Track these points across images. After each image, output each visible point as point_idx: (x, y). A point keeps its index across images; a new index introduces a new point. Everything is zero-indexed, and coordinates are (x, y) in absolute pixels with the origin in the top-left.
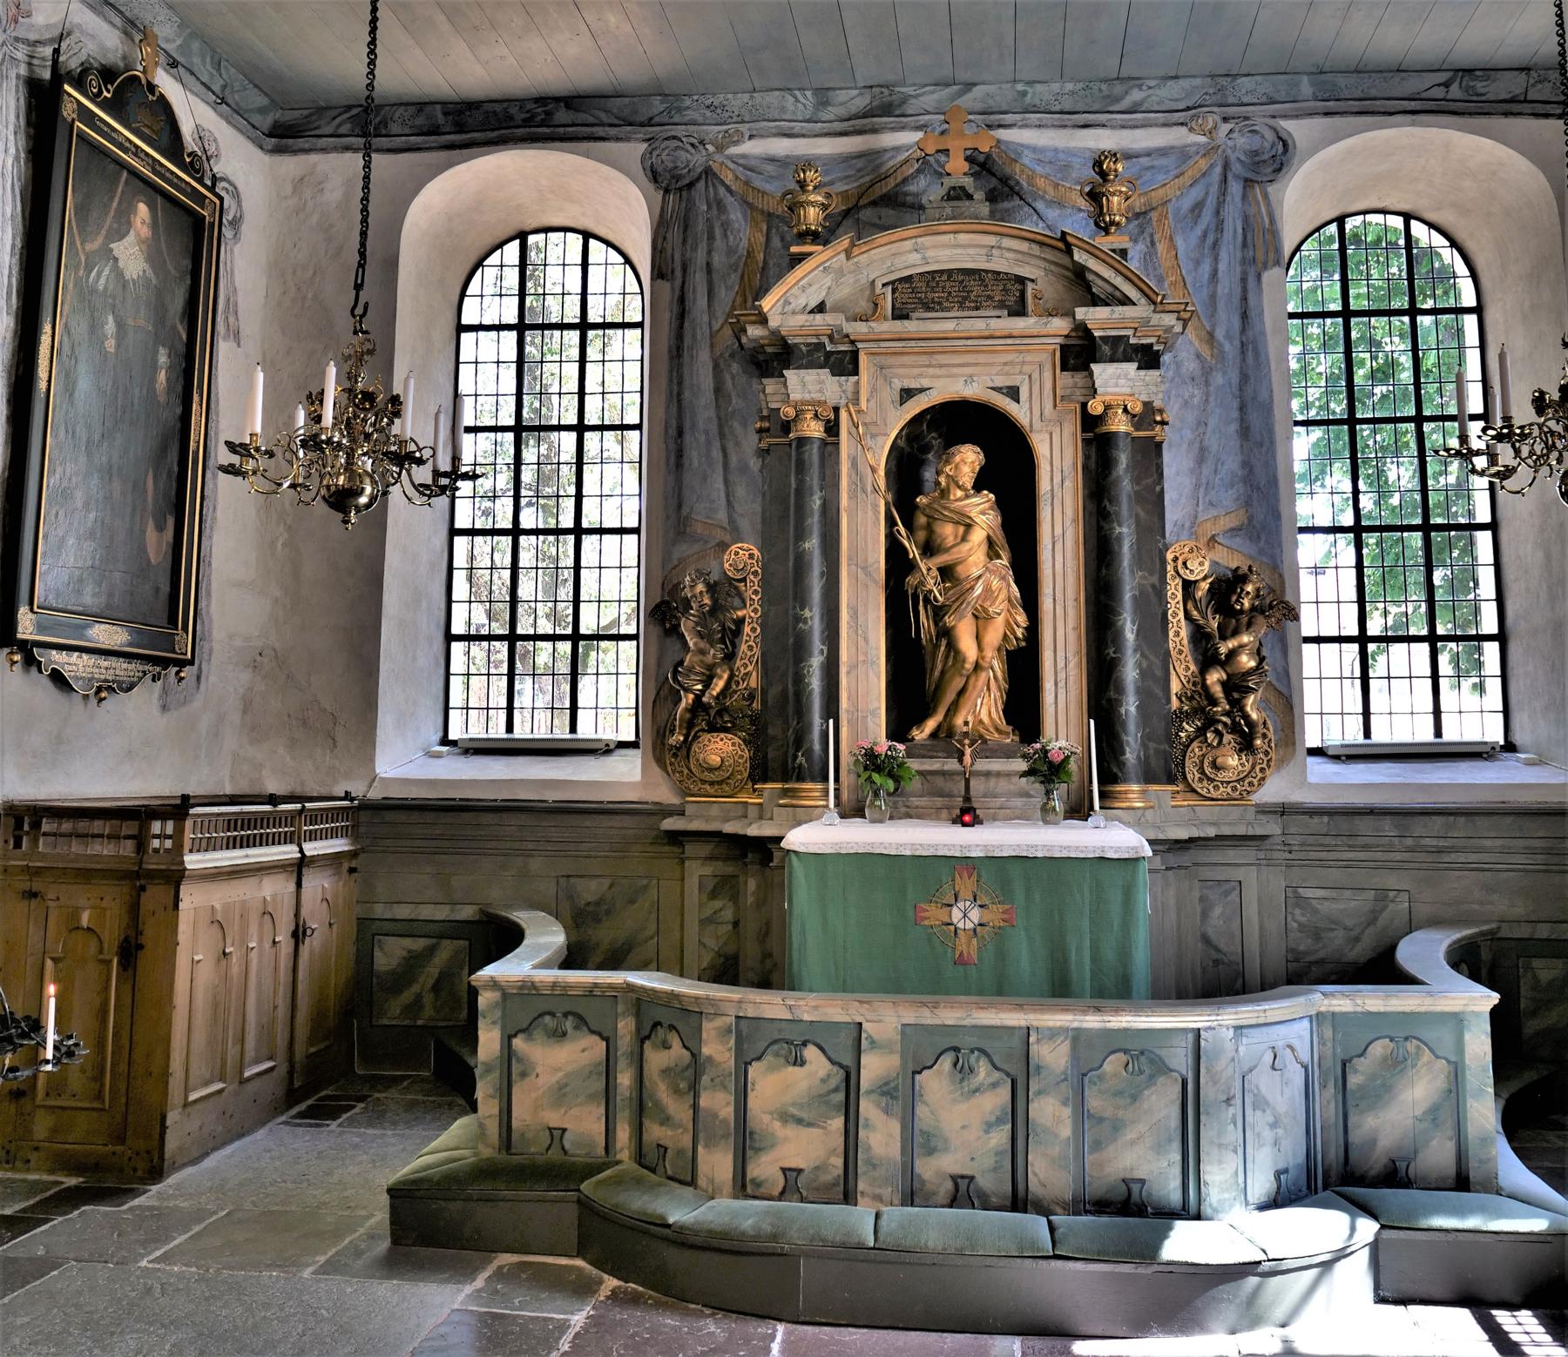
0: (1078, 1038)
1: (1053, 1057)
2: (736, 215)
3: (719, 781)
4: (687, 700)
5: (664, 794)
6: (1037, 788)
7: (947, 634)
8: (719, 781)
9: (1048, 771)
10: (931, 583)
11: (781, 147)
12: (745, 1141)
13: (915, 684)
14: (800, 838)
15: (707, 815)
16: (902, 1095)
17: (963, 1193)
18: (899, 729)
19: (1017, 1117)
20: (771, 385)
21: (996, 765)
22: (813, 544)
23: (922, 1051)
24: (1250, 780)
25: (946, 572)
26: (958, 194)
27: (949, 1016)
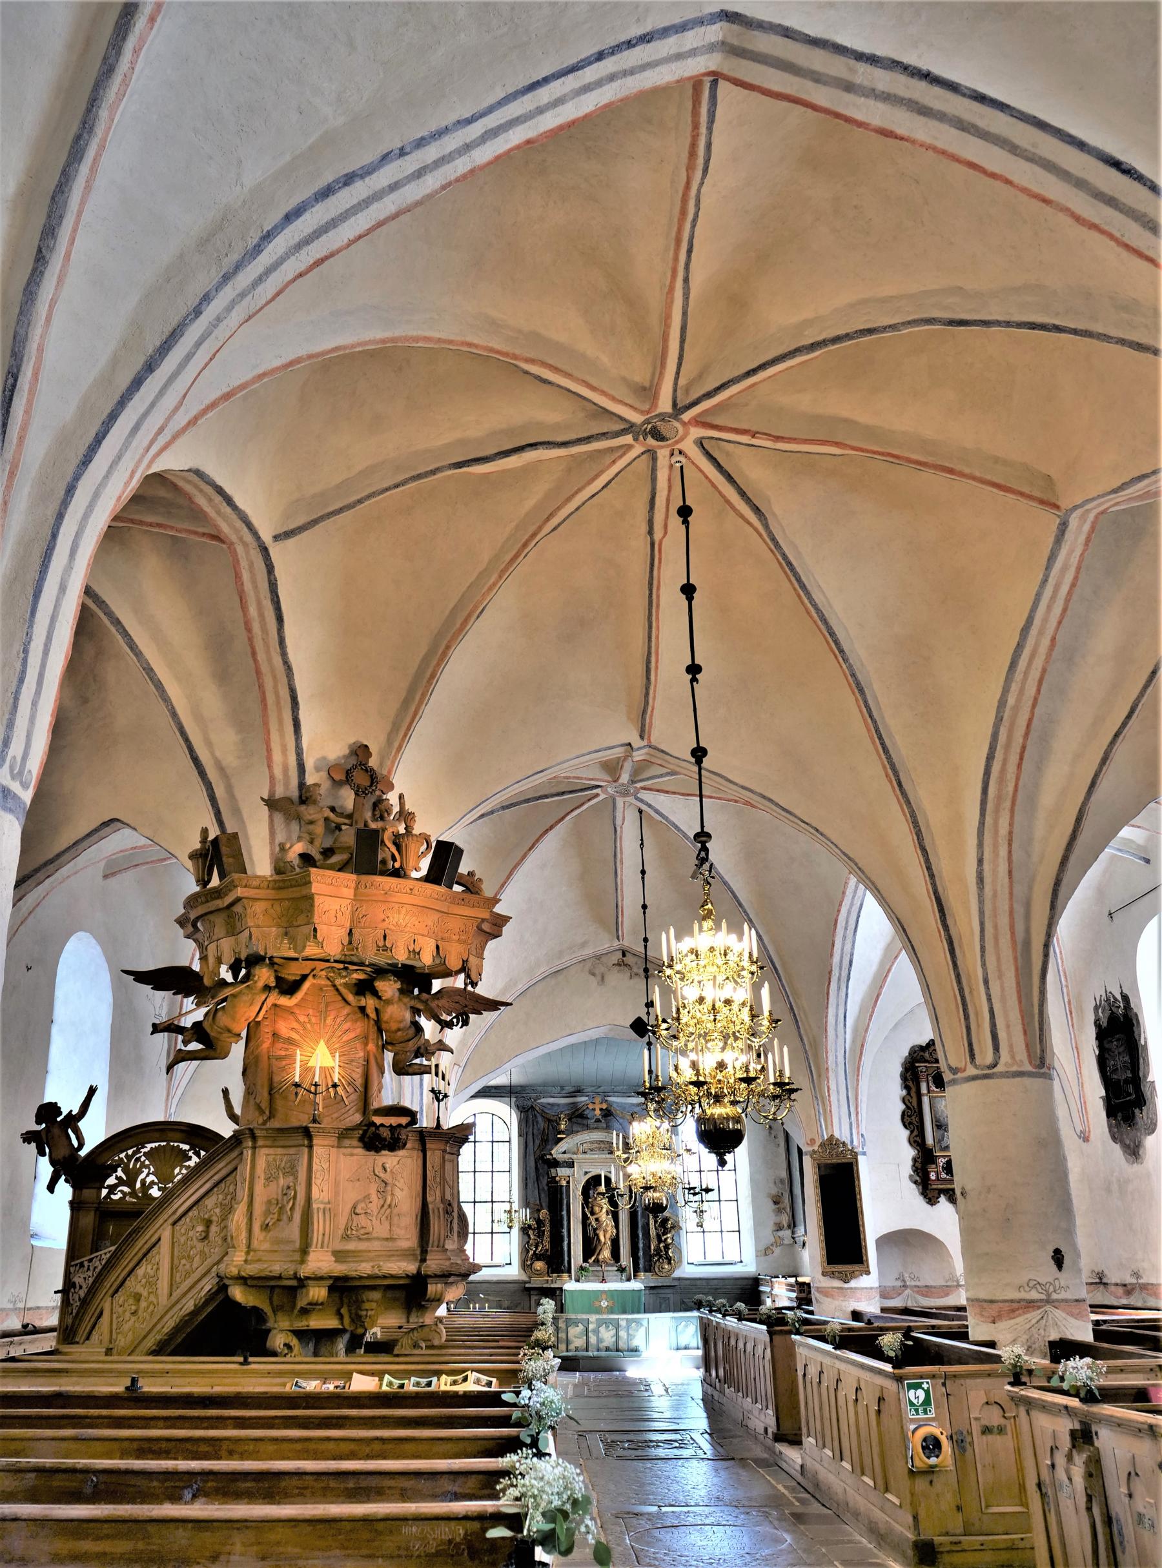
0: (627, 1320)
1: (623, 1323)
2: (540, 1119)
3: (539, 1274)
4: (531, 1252)
5: (524, 1278)
6: (619, 1273)
7: (597, 1235)
8: (539, 1274)
9: (622, 1270)
10: (594, 1223)
11: (551, 1100)
12: (568, 1342)
13: (590, 1248)
14: (566, 1287)
15: (537, 1282)
16: (596, 1332)
17: (608, 1349)
18: (585, 1260)
19: (617, 1335)
20: (553, 1170)
21: (609, 1268)
22: (564, 1213)
23: (600, 1322)
24: (671, 1271)
25: (597, 1220)
26: (598, 1121)
27: (605, 1316)
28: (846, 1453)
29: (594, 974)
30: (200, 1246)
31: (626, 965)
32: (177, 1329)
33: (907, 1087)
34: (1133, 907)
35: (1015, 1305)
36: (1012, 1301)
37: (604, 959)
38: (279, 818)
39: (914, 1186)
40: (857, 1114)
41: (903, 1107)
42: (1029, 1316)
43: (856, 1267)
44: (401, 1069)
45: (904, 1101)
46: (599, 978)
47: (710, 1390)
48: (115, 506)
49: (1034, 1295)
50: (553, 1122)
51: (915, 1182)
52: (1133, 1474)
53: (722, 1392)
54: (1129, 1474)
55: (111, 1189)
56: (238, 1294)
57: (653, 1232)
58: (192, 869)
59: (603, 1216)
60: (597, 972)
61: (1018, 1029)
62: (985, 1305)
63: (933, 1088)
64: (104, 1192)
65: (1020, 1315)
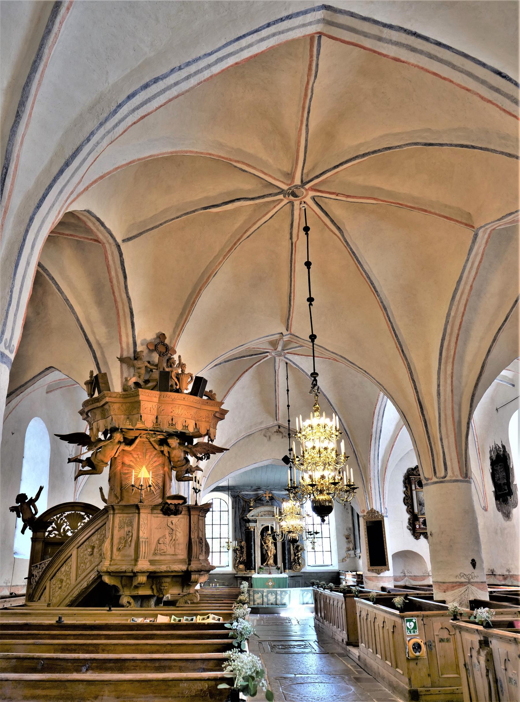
0: (281, 591)
1: (279, 592)
2: (241, 501)
3: (241, 570)
4: (238, 561)
5: (235, 572)
6: (277, 570)
7: (267, 553)
8: (241, 570)
9: (278, 569)
10: (266, 548)
11: (247, 493)
12: (254, 601)
13: (264, 559)
14: (253, 576)
15: (240, 574)
16: (267, 596)
17: (272, 604)
18: (262, 564)
19: (276, 598)
20: (247, 524)
21: (273, 568)
22: (253, 543)
23: (269, 592)
24: (300, 569)
25: (267, 546)
26: (268, 502)
27: (271, 589)
28: (379, 651)
29: (266, 436)
30: (89, 558)
31: (280, 432)
32: (79, 595)
33: (406, 487)
34: (507, 406)
35: (454, 584)
36: (453, 582)
37: (270, 429)
38: (125, 366)
39: (409, 531)
40: (384, 499)
41: (404, 496)
42: (460, 589)
43: (383, 567)
44: (179, 479)
45: (404, 493)
46: (268, 438)
47: (318, 622)
48: (52, 226)
49: (463, 580)
50: (247, 502)
51: (410, 529)
52: (507, 660)
53: (323, 623)
54: (505, 660)
55: (50, 532)
56: (106, 579)
57: (292, 552)
58: (86, 389)
59: (270, 545)
60: (267, 435)
61: (455, 461)
62: (441, 584)
63: (418, 487)
64: (47, 534)
65: (456, 589)
